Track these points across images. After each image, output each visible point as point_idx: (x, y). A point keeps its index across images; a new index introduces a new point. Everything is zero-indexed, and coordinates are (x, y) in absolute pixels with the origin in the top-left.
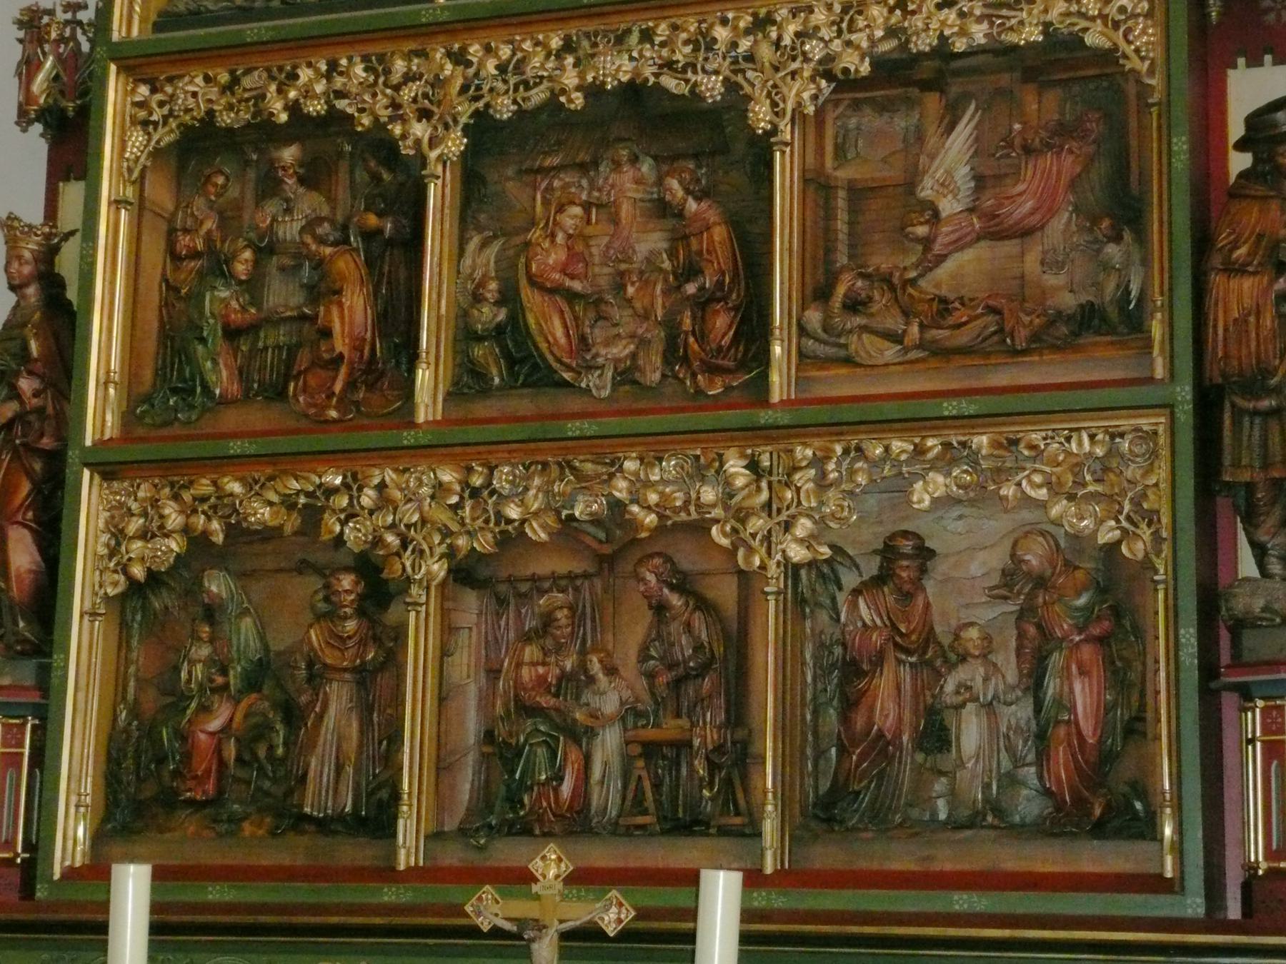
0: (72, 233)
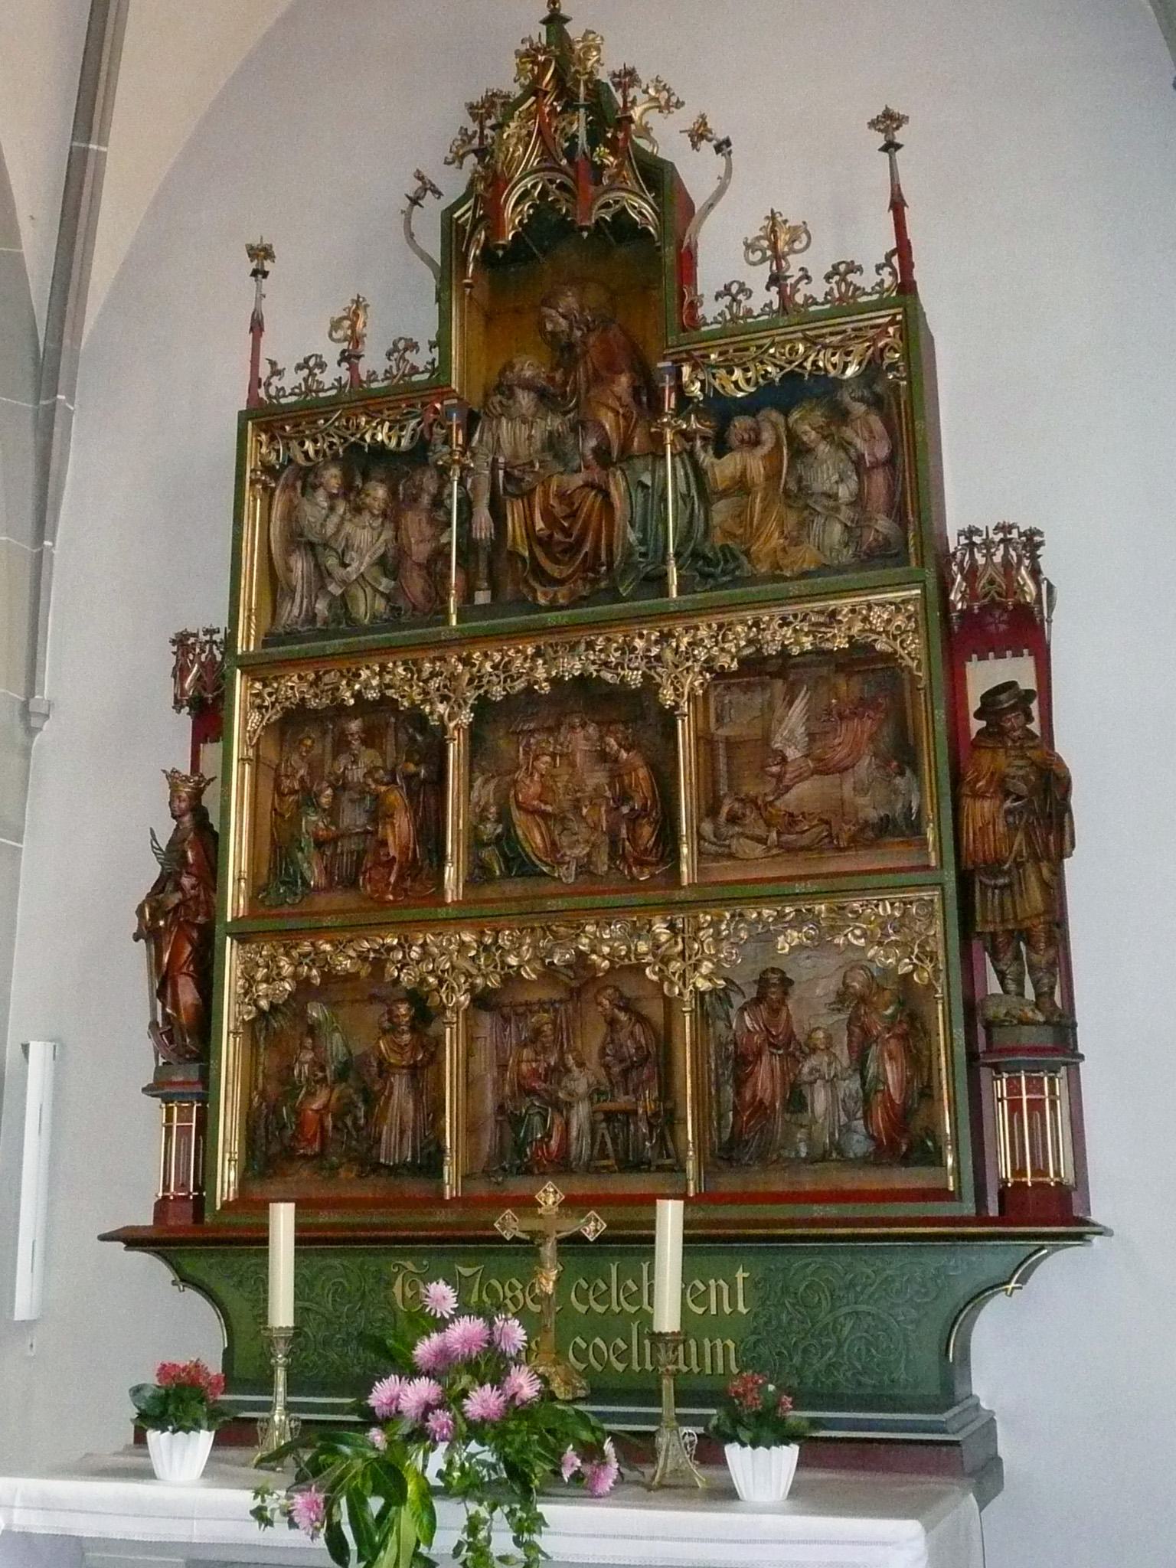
0: (212, 779)
